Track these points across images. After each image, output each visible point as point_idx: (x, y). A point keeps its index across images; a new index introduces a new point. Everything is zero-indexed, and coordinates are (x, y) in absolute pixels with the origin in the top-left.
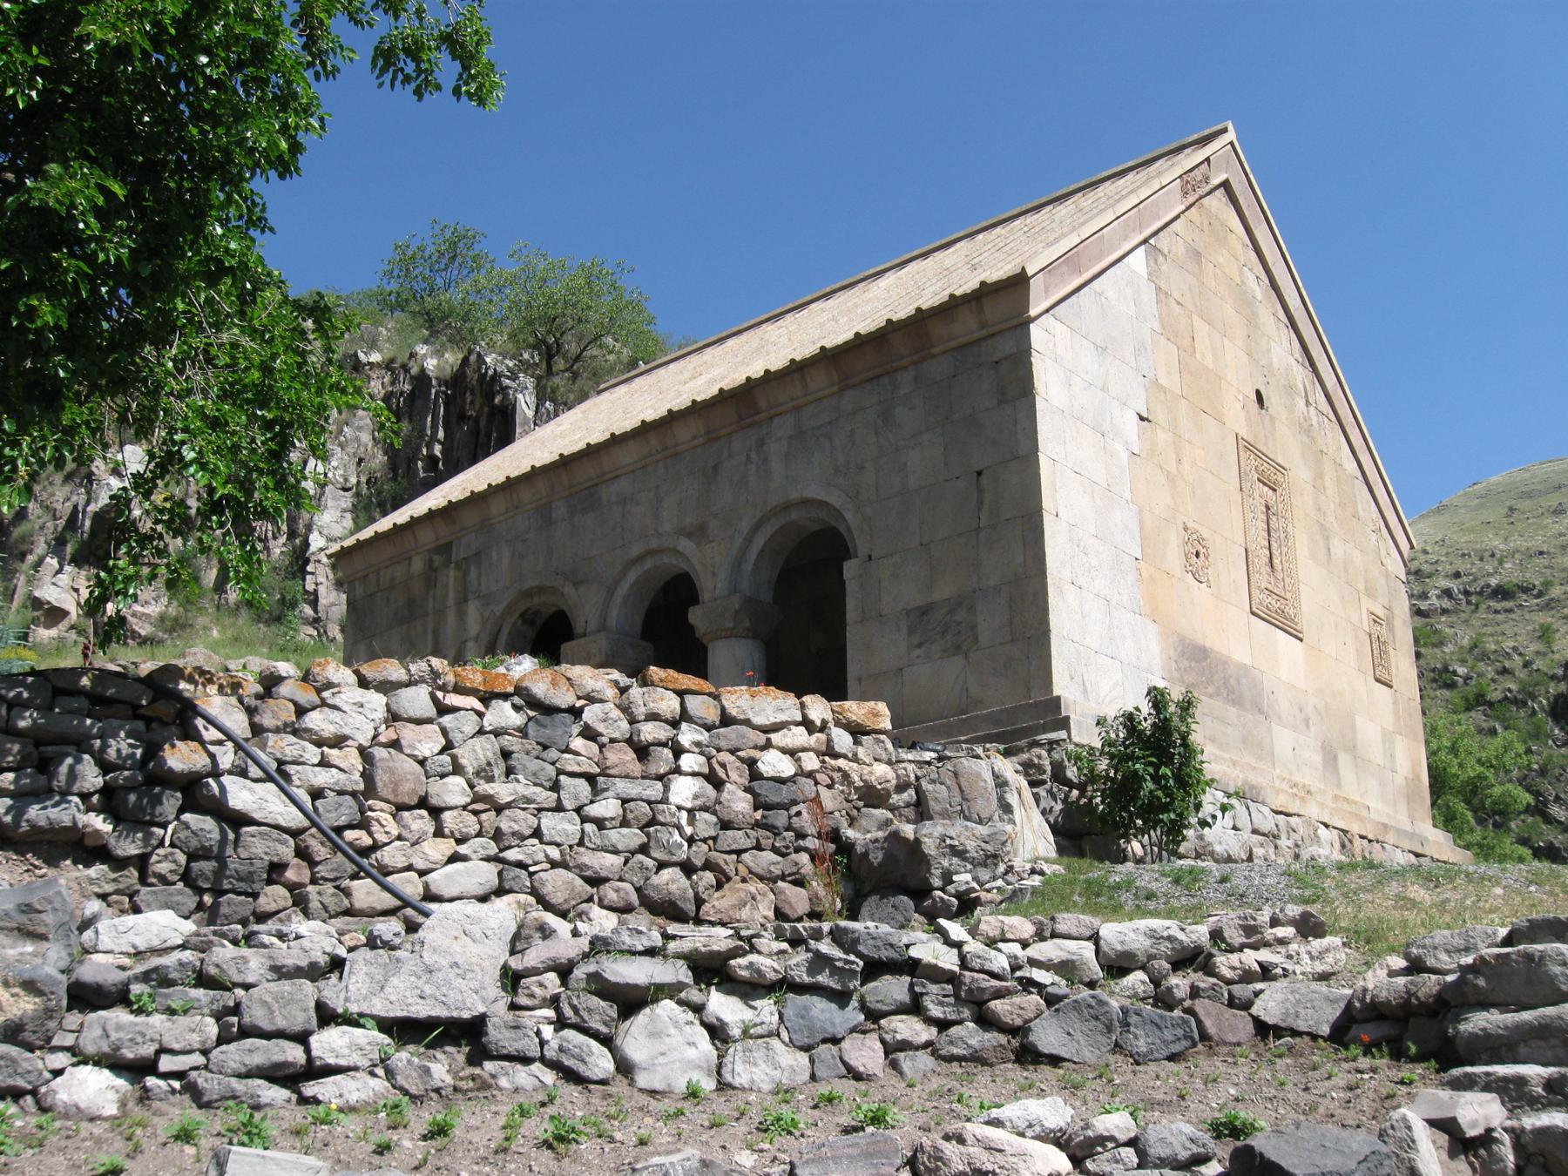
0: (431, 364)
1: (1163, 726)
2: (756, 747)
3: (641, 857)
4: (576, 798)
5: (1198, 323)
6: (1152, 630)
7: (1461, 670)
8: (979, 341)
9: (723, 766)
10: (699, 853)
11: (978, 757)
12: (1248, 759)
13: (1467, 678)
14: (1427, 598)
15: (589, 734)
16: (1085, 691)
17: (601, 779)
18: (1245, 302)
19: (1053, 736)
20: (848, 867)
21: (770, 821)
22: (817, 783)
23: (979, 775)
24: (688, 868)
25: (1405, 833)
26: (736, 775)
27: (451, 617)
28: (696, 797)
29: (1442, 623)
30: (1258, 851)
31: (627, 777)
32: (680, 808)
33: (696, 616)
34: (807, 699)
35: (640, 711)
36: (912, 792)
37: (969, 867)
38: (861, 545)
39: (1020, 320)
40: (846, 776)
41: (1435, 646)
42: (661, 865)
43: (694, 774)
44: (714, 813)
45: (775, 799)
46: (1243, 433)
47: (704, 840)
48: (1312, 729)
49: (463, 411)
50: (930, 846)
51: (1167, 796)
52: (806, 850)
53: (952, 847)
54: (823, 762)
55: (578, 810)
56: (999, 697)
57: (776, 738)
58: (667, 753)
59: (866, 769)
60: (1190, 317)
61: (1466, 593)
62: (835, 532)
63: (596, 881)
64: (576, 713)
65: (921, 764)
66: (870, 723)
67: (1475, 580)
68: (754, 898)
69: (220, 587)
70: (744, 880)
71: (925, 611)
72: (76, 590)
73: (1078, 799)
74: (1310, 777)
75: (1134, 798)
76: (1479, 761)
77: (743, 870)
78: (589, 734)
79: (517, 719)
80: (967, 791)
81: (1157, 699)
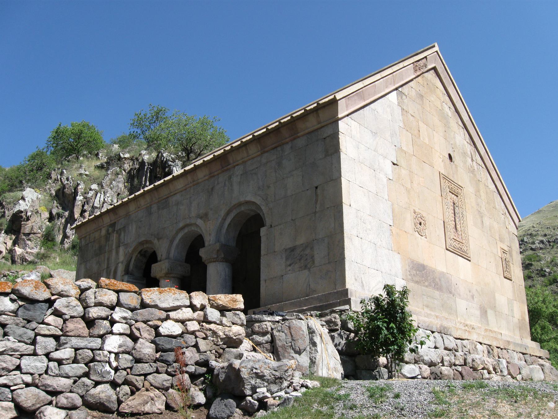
0: (146, 158)
1: (392, 303)
2: (159, 319)
3: (85, 379)
4: (45, 348)
5: (421, 124)
6: (397, 257)
7: (548, 270)
8: (317, 130)
9: (138, 329)
10: (121, 376)
11: (301, 319)
12: (445, 314)
13: (550, 273)
14: (534, 244)
15: (57, 314)
16: (363, 286)
17: (62, 338)
18: (443, 117)
19: (342, 308)
20: (211, 381)
21: (164, 358)
22: (196, 337)
23: (300, 328)
24: (114, 385)
25: (518, 344)
26: (146, 334)
27: (114, 252)
28: (120, 346)
29: (540, 253)
30: (446, 358)
31: (79, 336)
32: (110, 352)
33: (202, 253)
34: (193, 294)
35: (91, 301)
36: (269, 336)
37: (266, 384)
38: (268, 221)
39: (334, 120)
40: (214, 333)
41: (538, 261)
42: (97, 383)
43: (121, 334)
44: (132, 355)
45: (168, 346)
46: (443, 171)
47: (125, 369)
48: (475, 299)
49: (156, 175)
50: (245, 374)
51: (393, 337)
52: (187, 372)
53: (256, 373)
54: (202, 326)
55: (47, 355)
56: (322, 288)
57: (172, 314)
58: (106, 323)
59: (227, 329)
60: (418, 122)
61: (549, 242)
62: (258, 215)
63: (55, 393)
64: (50, 302)
65: (274, 322)
66: (231, 306)
67: (552, 237)
68: (152, 399)
69: (62, 242)
70: (147, 390)
71: (293, 249)
72: (6, 243)
73: (354, 338)
74: (474, 322)
75: (378, 338)
76: (554, 306)
77: (147, 384)
78: (57, 314)
79: (12, 306)
80: (294, 336)
81: (389, 290)
